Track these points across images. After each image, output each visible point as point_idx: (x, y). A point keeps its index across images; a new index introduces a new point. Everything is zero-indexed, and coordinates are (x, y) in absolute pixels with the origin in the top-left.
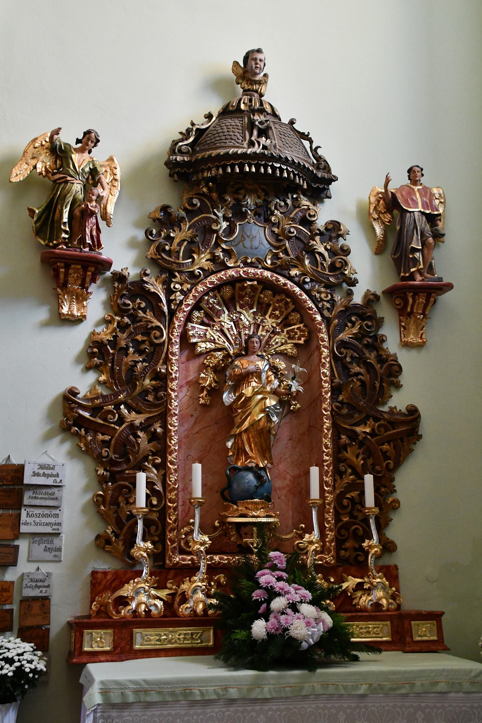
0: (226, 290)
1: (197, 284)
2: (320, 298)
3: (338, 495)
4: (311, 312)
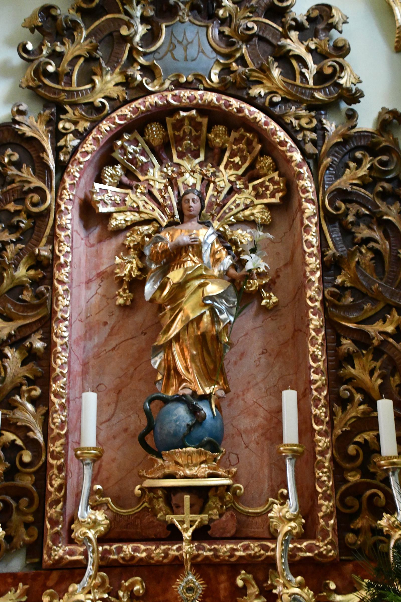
0: (152, 129)
1: (101, 121)
2: (300, 125)
3: (339, 438)
4: (284, 149)
